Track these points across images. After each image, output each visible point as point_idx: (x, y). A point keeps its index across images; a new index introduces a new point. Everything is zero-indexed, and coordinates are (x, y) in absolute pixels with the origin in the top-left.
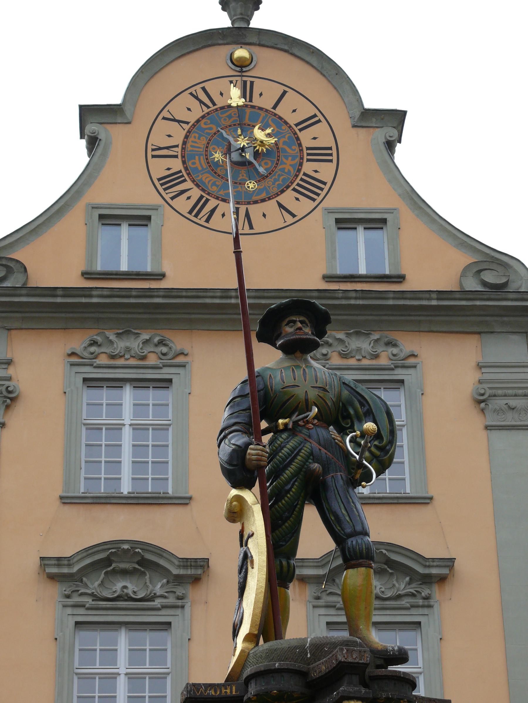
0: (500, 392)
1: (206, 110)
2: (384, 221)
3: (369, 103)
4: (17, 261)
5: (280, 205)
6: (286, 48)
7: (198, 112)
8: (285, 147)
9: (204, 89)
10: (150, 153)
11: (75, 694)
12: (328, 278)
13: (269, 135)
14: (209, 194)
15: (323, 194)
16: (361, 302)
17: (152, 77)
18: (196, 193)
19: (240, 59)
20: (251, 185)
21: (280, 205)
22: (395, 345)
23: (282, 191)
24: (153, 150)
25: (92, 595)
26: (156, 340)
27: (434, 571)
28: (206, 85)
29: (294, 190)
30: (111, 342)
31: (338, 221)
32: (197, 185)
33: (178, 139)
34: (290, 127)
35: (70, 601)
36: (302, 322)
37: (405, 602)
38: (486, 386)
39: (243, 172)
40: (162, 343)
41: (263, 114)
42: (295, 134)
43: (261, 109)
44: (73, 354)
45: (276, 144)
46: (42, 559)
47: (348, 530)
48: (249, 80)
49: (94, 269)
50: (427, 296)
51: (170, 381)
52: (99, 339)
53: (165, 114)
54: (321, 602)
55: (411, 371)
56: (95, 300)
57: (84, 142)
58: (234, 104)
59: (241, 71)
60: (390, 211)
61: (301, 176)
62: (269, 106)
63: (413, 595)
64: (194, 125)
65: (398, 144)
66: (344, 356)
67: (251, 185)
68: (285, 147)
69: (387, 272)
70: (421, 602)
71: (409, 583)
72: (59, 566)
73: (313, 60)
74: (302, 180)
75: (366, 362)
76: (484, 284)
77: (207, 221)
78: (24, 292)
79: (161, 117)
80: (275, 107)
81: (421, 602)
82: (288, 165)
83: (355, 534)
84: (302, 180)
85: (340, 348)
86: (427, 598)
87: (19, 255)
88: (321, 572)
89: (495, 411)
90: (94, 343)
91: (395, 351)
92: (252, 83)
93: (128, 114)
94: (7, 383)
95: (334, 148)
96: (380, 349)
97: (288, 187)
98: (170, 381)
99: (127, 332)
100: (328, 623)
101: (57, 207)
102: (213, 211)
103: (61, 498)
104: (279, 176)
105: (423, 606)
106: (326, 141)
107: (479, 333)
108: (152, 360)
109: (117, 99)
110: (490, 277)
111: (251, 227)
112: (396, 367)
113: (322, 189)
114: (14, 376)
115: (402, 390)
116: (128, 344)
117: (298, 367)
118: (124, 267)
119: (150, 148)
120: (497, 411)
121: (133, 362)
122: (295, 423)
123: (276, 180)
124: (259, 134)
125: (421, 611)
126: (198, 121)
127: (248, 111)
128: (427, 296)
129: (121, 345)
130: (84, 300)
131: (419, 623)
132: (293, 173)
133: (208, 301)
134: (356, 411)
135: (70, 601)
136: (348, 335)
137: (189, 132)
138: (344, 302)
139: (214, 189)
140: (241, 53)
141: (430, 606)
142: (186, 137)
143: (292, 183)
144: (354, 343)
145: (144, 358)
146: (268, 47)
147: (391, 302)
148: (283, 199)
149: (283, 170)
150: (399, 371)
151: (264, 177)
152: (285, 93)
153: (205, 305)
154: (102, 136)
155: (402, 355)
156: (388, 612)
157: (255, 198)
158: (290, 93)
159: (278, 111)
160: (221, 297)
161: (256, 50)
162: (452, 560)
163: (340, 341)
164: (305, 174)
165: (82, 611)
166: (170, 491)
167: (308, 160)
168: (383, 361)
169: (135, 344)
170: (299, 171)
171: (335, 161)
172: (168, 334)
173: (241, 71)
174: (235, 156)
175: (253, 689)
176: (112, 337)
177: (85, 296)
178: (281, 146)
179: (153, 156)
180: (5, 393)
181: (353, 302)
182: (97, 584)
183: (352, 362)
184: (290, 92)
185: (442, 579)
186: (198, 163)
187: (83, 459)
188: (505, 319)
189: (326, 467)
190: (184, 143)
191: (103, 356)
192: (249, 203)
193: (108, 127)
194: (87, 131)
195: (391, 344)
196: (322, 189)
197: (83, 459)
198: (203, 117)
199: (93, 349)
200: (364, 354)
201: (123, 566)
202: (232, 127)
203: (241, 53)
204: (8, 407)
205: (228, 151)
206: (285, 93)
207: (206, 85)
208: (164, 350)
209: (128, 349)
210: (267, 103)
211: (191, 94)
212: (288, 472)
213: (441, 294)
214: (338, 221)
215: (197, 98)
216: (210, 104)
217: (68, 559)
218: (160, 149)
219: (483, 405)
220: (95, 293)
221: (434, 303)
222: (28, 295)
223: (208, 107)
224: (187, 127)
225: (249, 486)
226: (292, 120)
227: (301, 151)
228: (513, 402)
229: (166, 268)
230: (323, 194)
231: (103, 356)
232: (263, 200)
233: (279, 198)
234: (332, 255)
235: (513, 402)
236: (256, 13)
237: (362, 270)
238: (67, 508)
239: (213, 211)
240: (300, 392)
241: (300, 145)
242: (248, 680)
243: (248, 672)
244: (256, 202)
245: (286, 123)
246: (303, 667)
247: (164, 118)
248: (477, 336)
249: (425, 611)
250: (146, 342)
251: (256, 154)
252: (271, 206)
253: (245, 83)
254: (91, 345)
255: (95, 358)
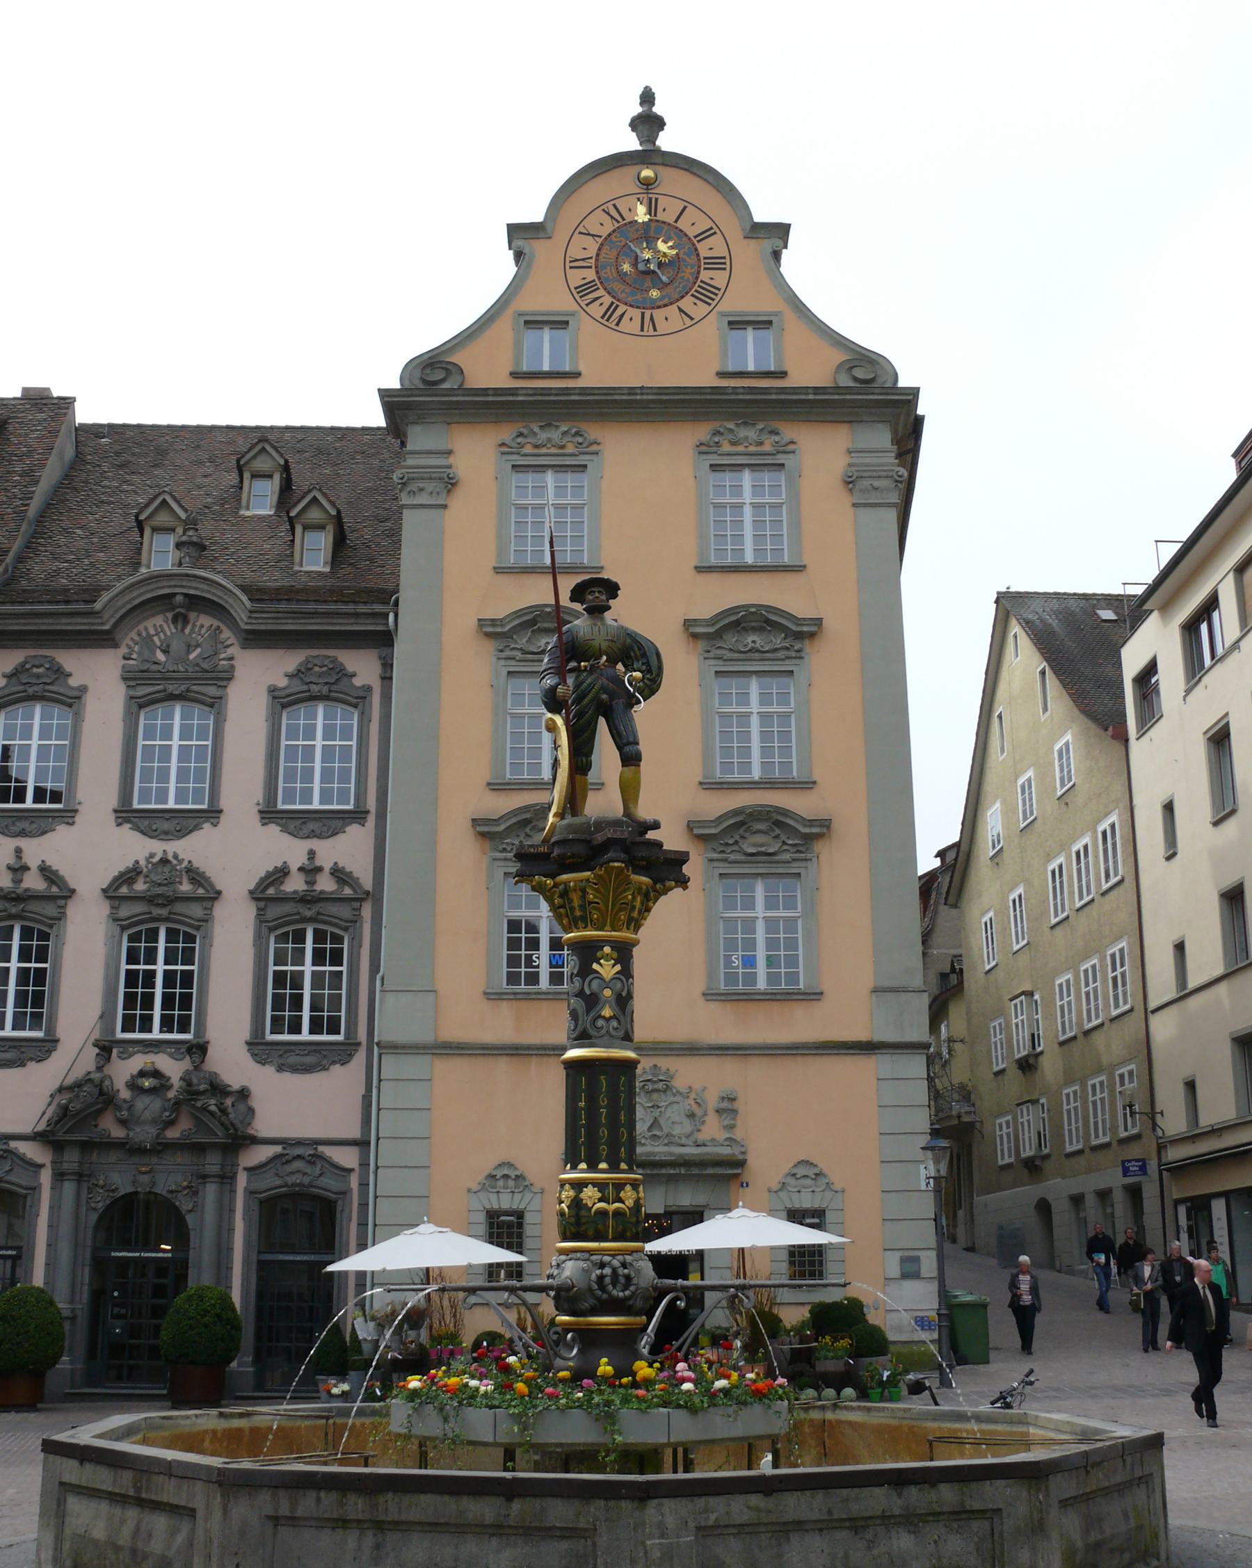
0: (866, 474)
1: (617, 225)
2: (770, 323)
3: (758, 218)
4: (455, 364)
5: (680, 310)
6: (686, 167)
7: (609, 226)
8: (685, 257)
9: (614, 206)
10: (568, 265)
11: (509, 730)
12: (722, 375)
13: (671, 248)
14: (618, 300)
15: (717, 298)
16: (748, 397)
17: (569, 196)
18: (607, 300)
19: (646, 178)
20: (655, 293)
21: (680, 310)
22: (777, 434)
23: (682, 297)
24: (571, 262)
25: (521, 649)
26: (573, 431)
27: (805, 629)
28: (616, 202)
29: (693, 295)
30: (535, 434)
31: (730, 323)
32: (609, 293)
33: (592, 252)
34: (690, 239)
35: (503, 655)
36: (599, 592)
37: (781, 654)
38: (854, 469)
39: (648, 281)
40: (577, 434)
41: (666, 227)
42: (694, 245)
43: (664, 223)
44: (503, 444)
45: (677, 254)
46: (479, 620)
47: (625, 741)
48: (654, 197)
49: (519, 370)
50: (804, 391)
51: (585, 466)
52: (525, 431)
53: (581, 229)
54: (711, 655)
55: (791, 456)
56: (521, 398)
57: (511, 252)
58: (640, 221)
59: (647, 189)
60: (776, 314)
61: (698, 283)
62: (671, 220)
63: (787, 649)
64: (606, 239)
65: (784, 251)
66: (733, 444)
67: (655, 294)
68: (685, 257)
69: (772, 369)
70: (793, 654)
71: (785, 638)
72: (493, 626)
73: (710, 179)
74: (699, 286)
75: (752, 449)
76: (856, 379)
77: (617, 324)
78: (460, 392)
79: (577, 231)
80: (676, 221)
81: (793, 654)
82: (687, 273)
83: (629, 743)
84: (699, 286)
85: (730, 437)
86: (799, 651)
87: (454, 358)
88: (711, 630)
89: (861, 490)
90: (521, 435)
91: (777, 438)
92: (656, 199)
93: (549, 230)
94: (448, 471)
95: (728, 257)
96: (764, 437)
97: (687, 293)
98: (585, 466)
99: (549, 425)
100: (716, 672)
101: (487, 316)
102: (622, 316)
103: (495, 568)
104: (680, 283)
105: (795, 658)
106: (720, 251)
107: (850, 422)
108: (570, 449)
109: (538, 217)
110: (860, 373)
111: (655, 330)
112: (778, 452)
113: (716, 295)
114: (454, 465)
115: (783, 472)
116: (549, 436)
117: (595, 625)
118: (546, 368)
119: (568, 259)
120: (863, 491)
121: (553, 451)
122: (592, 666)
123: (677, 287)
124: (662, 246)
125: (794, 662)
126: (609, 235)
127: (653, 225)
128: (804, 391)
129: (543, 436)
130: (511, 398)
131: (792, 671)
132: (691, 280)
133: (617, 397)
134: (636, 655)
135: (503, 655)
136: (737, 425)
137: (602, 245)
138: (733, 397)
139: (622, 296)
140: (647, 173)
141: (801, 658)
142: (599, 249)
143: (691, 289)
144: (743, 432)
145: (562, 447)
146: (671, 166)
147: (774, 397)
148: (682, 304)
149: (682, 278)
150: (780, 456)
151: (667, 285)
152: (685, 208)
153: (615, 401)
154: (526, 251)
155: (783, 443)
156: (766, 663)
157: (658, 303)
158: (690, 208)
159: (680, 225)
160: (629, 394)
161: (660, 169)
162: (820, 620)
163: (731, 431)
164: (702, 281)
165: (513, 663)
166: (585, 562)
167: (705, 269)
168: (767, 448)
169: (555, 435)
170: (697, 278)
171: (728, 269)
172: (584, 426)
173: (647, 189)
174: (641, 267)
175: (556, 852)
176: (536, 430)
177: (513, 395)
178: (681, 256)
179: (571, 267)
180: (447, 480)
181: (741, 397)
182: (525, 640)
183: (740, 449)
184: (690, 207)
185: (812, 635)
186: (609, 273)
187: (513, 534)
188: (873, 410)
189: (612, 696)
190: (598, 255)
191: (528, 446)
192: (653, 308)
193: (532, 241)
194: (513, 245)
195: (774, 432)
196: (716, 295)
197: (513, 534)
198: (614, 231)
199: (519, 440)
200: (750, 441)
201: (546, 625)
202: (637, 240)
203: (647, 173)
204: (449, 491)
205: (635, 264)
206: (685, 208)
207: (616, 202)
208: (580, 440)
209: (549, 440)
210: (669, 217)
211: (604, 210)
212: (586, 701)
213: (817, 390)
214: (730, 323)
215: (608, 214)
216: (620, 219)
217: (501, 620)
218: (576, 260)
219: (851, 486)
220: (520, 392)
221: (811, 397)
222: (463, 395)
223: (618, 222)
224: (600, 240)
225: (559, 713)
226: (692, 232)
227: (699, 260)
228: (876, 483)
229: (582, 367)
230: (717, 298)
231: (528, 446)
232: (665, 306)
233: (679, 304)
234: (724, 354)
235: (876, 483)
236: (661, 133)
237: (751, 367)
238: (499, 577)
239: (622, 316)
240: (596, 643)
241: (698, 255)
242: (554, 844)
243: (553, 840)
244: (659, 307)
245: (686, 235)
246: (588, 838)
247: (580, 233)
248: (847, 426)
249: (797, 661)
250: (565, 433)
251: (660, 265)
252: (672, 311)
253: (651, 199)
254: (518, 436)
255: (522, 447)
